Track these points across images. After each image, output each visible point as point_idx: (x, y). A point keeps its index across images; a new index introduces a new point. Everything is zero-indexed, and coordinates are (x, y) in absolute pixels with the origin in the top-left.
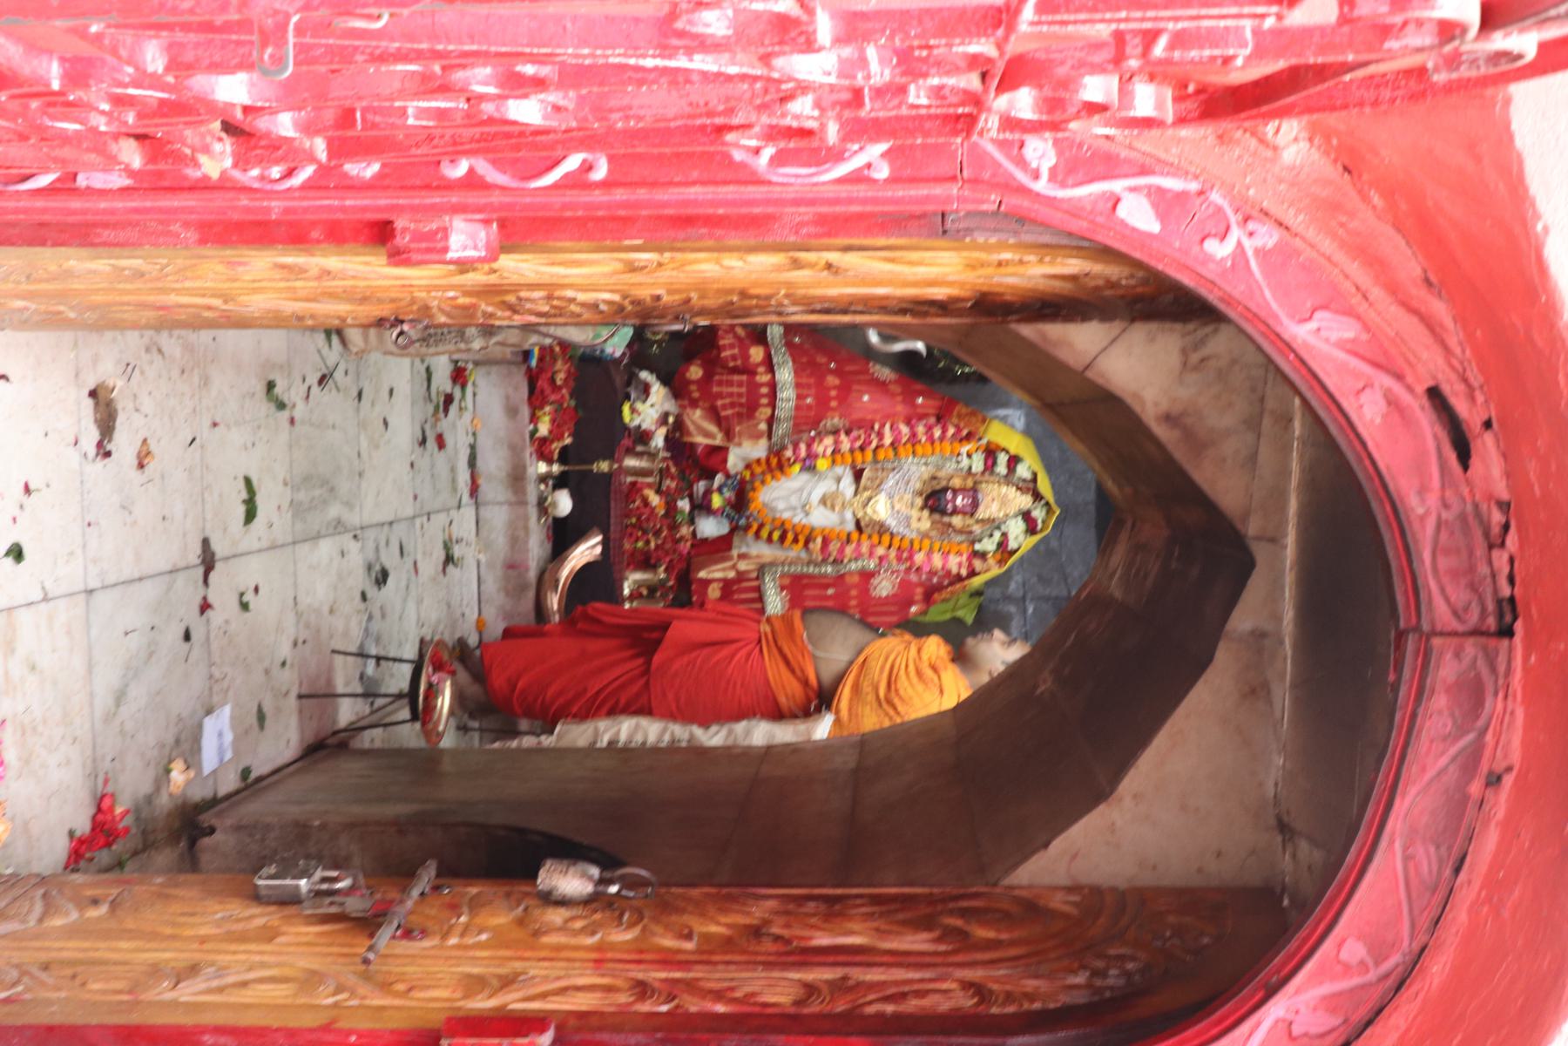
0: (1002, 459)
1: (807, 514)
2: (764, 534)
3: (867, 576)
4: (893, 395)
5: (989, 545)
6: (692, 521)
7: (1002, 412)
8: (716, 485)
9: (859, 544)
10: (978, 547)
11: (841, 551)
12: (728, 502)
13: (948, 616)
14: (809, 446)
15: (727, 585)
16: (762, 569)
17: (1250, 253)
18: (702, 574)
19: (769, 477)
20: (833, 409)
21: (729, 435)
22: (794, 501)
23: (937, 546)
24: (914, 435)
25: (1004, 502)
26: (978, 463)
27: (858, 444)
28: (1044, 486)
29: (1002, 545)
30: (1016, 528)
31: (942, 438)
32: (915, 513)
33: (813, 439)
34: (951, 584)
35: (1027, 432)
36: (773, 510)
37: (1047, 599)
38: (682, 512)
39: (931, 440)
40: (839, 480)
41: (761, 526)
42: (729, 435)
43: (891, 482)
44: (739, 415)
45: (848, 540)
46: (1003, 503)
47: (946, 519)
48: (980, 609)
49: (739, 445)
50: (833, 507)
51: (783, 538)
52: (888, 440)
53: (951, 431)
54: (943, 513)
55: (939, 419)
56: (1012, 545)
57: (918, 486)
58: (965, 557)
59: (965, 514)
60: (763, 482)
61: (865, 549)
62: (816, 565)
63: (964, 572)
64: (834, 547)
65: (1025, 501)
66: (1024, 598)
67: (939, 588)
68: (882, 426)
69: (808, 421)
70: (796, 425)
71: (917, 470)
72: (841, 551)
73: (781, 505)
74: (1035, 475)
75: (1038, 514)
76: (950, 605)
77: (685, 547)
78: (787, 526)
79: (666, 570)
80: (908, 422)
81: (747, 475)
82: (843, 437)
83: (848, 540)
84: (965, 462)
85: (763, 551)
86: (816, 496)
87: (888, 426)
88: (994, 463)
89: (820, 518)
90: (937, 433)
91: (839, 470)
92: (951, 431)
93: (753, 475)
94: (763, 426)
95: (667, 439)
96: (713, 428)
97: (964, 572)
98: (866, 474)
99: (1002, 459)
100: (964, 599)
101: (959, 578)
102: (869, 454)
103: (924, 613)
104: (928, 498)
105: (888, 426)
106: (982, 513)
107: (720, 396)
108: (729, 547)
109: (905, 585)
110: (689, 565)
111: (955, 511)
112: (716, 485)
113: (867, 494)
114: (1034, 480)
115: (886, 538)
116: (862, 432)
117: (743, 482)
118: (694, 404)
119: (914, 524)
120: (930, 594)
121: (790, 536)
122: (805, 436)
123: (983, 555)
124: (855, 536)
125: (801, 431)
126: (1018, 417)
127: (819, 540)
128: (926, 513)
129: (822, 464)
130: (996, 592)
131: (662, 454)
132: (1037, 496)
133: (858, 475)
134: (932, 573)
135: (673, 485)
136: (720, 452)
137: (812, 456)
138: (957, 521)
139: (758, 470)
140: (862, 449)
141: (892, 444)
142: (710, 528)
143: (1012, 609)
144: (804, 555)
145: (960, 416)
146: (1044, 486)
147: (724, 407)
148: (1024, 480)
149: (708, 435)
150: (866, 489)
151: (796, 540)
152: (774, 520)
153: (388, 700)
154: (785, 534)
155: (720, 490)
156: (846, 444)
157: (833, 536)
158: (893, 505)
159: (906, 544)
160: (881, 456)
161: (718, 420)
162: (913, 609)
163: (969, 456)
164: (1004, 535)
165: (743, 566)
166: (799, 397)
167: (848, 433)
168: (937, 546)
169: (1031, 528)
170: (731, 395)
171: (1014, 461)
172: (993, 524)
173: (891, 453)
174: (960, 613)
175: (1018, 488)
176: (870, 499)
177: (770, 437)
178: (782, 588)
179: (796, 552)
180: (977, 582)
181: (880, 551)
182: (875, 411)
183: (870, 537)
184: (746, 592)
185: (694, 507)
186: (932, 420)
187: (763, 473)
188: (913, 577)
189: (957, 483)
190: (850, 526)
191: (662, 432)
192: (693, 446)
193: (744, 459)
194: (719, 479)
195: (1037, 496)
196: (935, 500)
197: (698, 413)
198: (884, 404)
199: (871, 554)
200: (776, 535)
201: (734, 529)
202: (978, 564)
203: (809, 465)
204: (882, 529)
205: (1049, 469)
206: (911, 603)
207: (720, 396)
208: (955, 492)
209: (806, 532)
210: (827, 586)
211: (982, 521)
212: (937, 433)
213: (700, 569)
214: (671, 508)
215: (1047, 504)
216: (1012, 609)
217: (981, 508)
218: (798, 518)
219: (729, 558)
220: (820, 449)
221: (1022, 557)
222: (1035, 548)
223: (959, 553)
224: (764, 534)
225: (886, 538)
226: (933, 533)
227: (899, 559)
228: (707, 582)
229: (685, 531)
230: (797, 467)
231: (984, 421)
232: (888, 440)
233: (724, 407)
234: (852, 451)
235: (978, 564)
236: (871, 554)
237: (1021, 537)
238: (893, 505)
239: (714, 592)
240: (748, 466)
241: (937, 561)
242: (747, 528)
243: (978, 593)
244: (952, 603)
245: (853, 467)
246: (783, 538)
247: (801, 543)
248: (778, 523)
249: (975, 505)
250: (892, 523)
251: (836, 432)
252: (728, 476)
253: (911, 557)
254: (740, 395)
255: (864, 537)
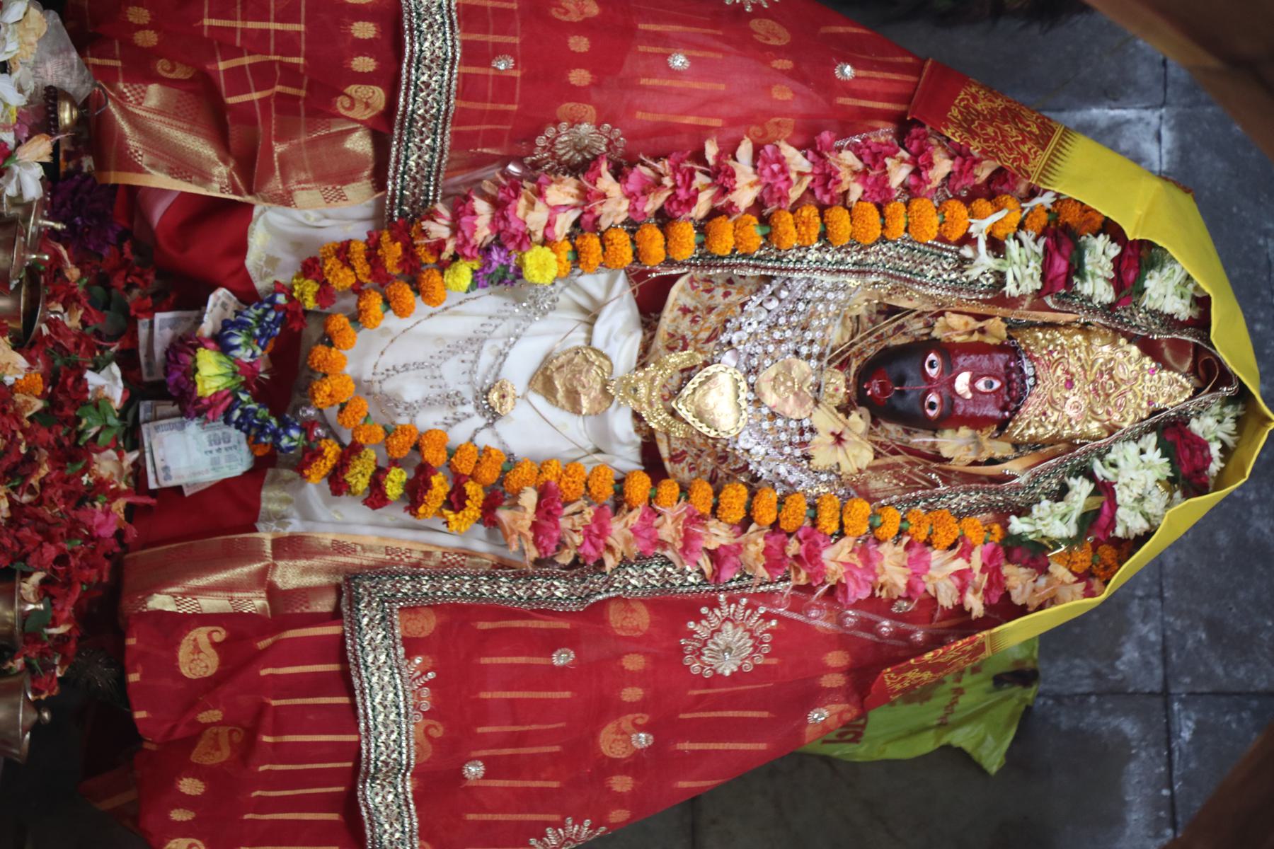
0: (1100, 255)
1: (493, 416)
2: (359, 478)
3: (676, 611)
4: (764, 52)
5: (1053, 522)
6: (132, 437)
7: (1101, 114)
8: (208, 326)
9: (652, 512)
10: (1018, 525)
11: (596, 533)
12: (247, 377)
13: (926, 745)
14: (500, 207)
15: (239, 634)
16: (348, 586)
17: (787, 614)
18: (161, 602)
19: (375, 302)
20: (577, 94)
21: (250, 168)
22: (453, 375)
23: (892, 520)
24: (826, 177)
25: (1104, 386)
26: (1023, 270)
27: (653, 204)
28: (1231, 340)
29: (1096, 521)
30: (1139, 471)
31: (911, 191)
32: (825, 420)
33: (515, 186)
34: (935, 641)
35: (1181, 176)
36: (389, 401)
37: (1237, 697)
38: (99, 404)
39: (880, 196)
40: (591, 316)
41: (351, 451)
42: (250, 168)
43: (753, 321)
44: (286, 105)
45: (620, 502)
46: (1096, 388)
47: (921, 440)
48: (1027, 720)
49: (286, 200)
50: (573, 399)
51: (415, 494)
52: (744, 196)
53: (943, 166)
54: (914, 420)
55: (905, 128)
56: (1129, 521)
57: (837, 335)
58: (977, 559)
59: (976, 423)
60: (357, 318)
61: (668, 530)
62: (520, 574)
63: (975, 604)
64: (573, 523)
65: (1168, 388)
66: (1165, 695)
67: (899, 652)
68: (730, 150)
69: (503, 137)
70: (460, 141)
71: (834, 297)
72: (596, 533)
73: (412, 389)
74: (1202, 303)
75: (1210, 427)
76: (931, 711)
77: (109, 516)
78: (433, 456)
79: (44, 590)
80: (808, 144)
81: (308, 292)
82: (607, 182)
83: (620, 502)
84: (985, 261)
85: (355, 529)
86: (521, 363)
87: (745, 151)
88: (1077, 269)
89: (534, 431)
90: (899, 174)
91: (593, 283)
92: (943, 166)
93: (325, 294)
94: (359, 143)
95: (51, 173)
96: (201, 147)
97: (975, 604)
98: (677, 295)
99: (1100, 255)
100: (975, 692)
101: (961, 621)
102: (687, 235)
103: (852, 731)
104: (864, 375)
105: (745, 151)
106: (1032, 421)
107: (225, 44)
108: (249, 517)
109: (791, 639)
110: (118, 568)
111: (951, 418)
112: (208, 326)
113: (677, 359)
114: (1201, 323)
115: (735, 497)
116: (664, 166)
117: (294, 314)
118: (141, 72)
119: (824, 455)
120: (869, 671)
121: (440, 485)
122: (489, 177)
123: (1034, 554)
124: (640, 486)
125: (481, 162)
126: (1151, 128)
127: (529, 498)
128: (859, 421)
129: (541, 265)
130: (1075, 675)
131: (37, 223)
132: (1209, 373)
133: (651, 299)
134: (877, 605)
135: (72, 321)
136: (228, 218)
137: (511, 238)
138: (955, 445)
139: (342, 279)
140: (665, 219)
141: (759, 204)
142: (190, 455)
143: (1129, 727)
144: (479, 543)
145: (967, 125)
146: (1231, 340)
147: (238, 80)
148: (1170, 321)
149: (182, 166)
150: (677, 343)
151: (456, 500)
152: (389, 432)
153: (583, 453)
154: (423, 476)
155: (221, 342)
156: (615, 209)
157: (572, 487)
158: (758, 392)
159: (796, 515)
160: (724, 241)
161: (219, 123)
162: (818, 716)
163: (996, 246)
164: (1104, 490)
165: (289, 575)
166: (474, 54)
167: (619, 174)
168: (892, 520)
169: (1188, 474)
170: (258, 41)
171: (1137, 259)
172: (1072, 457)
173: (754, 233)
174: (960, 737)
175: (1149, 348)
176: (687, 373)
177: (379, 180)
178: (412, 646)
179: (460, 535)
180: (1015, 635)
181: (718, 535)
182: (709, 103)
183: (685, 490)
184: (294, 656)
185: (137, 390)
186: (884, 133)
187: (358, 289)
188: (819, 620)
189: (956, 327)
190: (627, 458)
191: (40, 148)
192: (136, 198)
193: (297, 244)
194: (219, 302)
195: (1209, 373)
196: (886, 380)
197: (154, 94)
198: (735, 82)
199: (689, 542)
200: (395, 482)
201: (265, 464)
202: (1018, 579)
203: (500, 275)
204: (724, 465)
205: (1246, 294)
206: (814, 697)
207: (225, 44)
208: (949, 351)
209: (489, 474)
210: (553, 641)
211: (1035, 445)
212: (899, 174)
213: (156, 587)
214: (65, 392)
215: (1243, 395)
216: (1129, 727)
217: (1030, 409)
218: (466, 430)
219: (250, 553)
220: (536, 219)
221: (1158, 563)
222: (1200, 533)
223: (960, 546)
224: (359, 478)
225: (735, 497)
226: (878, 484)
227: (774, 560)
228: (179, 624)
229: (106, 465)
230: (463, 274)
231: (1043, 140)
232: (744, 196)
233: (238, 80)
234: (632, 225)
235: (1018, 579)
236: (689, 542)
237: (1156, 503)
238: (758, 392)
239: (197, 658)
240: (311, 268)
241: (893, 568)
242: (311, 454)
243: (1020, 675)
244: (940, 700)
245: (637, 276)
246: (415, 494)
247: (473, 509)
248: (401, 446)
249: (1013, 395)
250: (754, 448)
251: (583, 168)
252: (247, 295)
253: (810, 557)
254: (287, 43)
255: (669, 489)
